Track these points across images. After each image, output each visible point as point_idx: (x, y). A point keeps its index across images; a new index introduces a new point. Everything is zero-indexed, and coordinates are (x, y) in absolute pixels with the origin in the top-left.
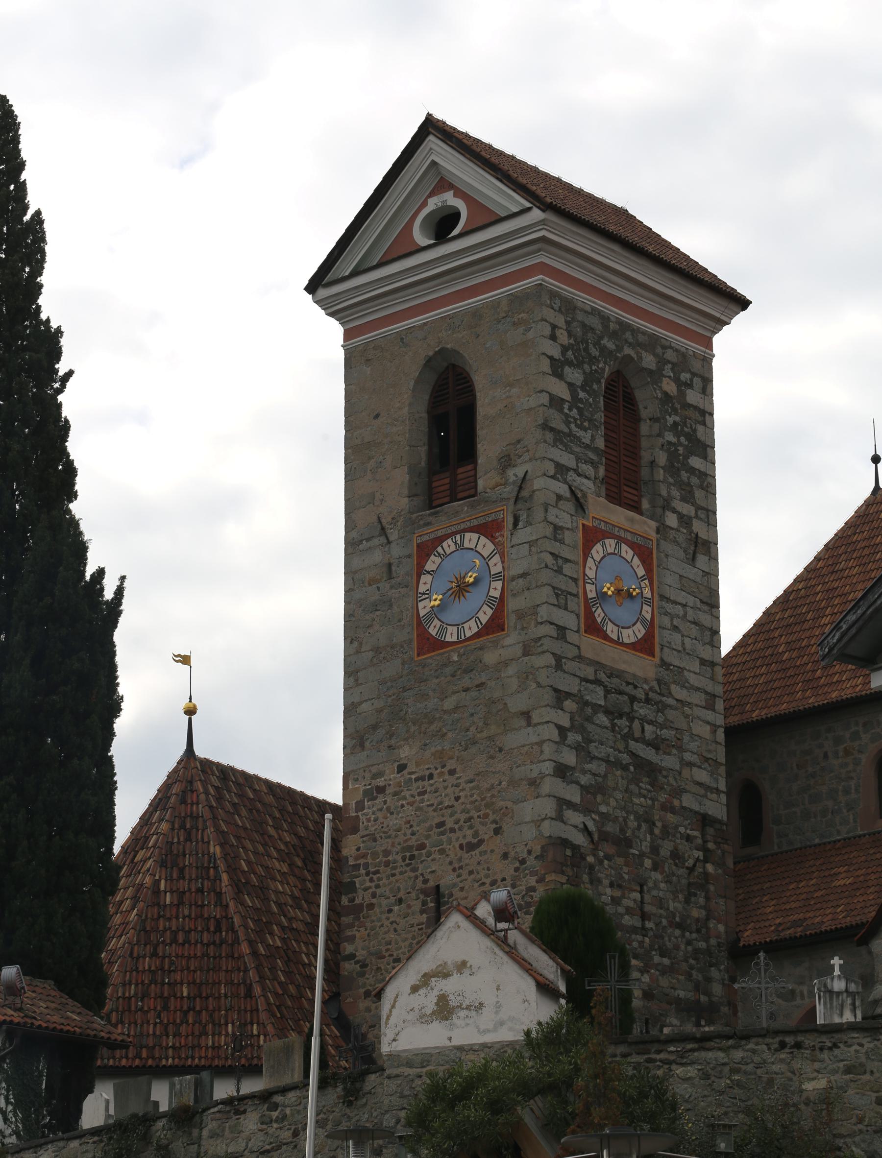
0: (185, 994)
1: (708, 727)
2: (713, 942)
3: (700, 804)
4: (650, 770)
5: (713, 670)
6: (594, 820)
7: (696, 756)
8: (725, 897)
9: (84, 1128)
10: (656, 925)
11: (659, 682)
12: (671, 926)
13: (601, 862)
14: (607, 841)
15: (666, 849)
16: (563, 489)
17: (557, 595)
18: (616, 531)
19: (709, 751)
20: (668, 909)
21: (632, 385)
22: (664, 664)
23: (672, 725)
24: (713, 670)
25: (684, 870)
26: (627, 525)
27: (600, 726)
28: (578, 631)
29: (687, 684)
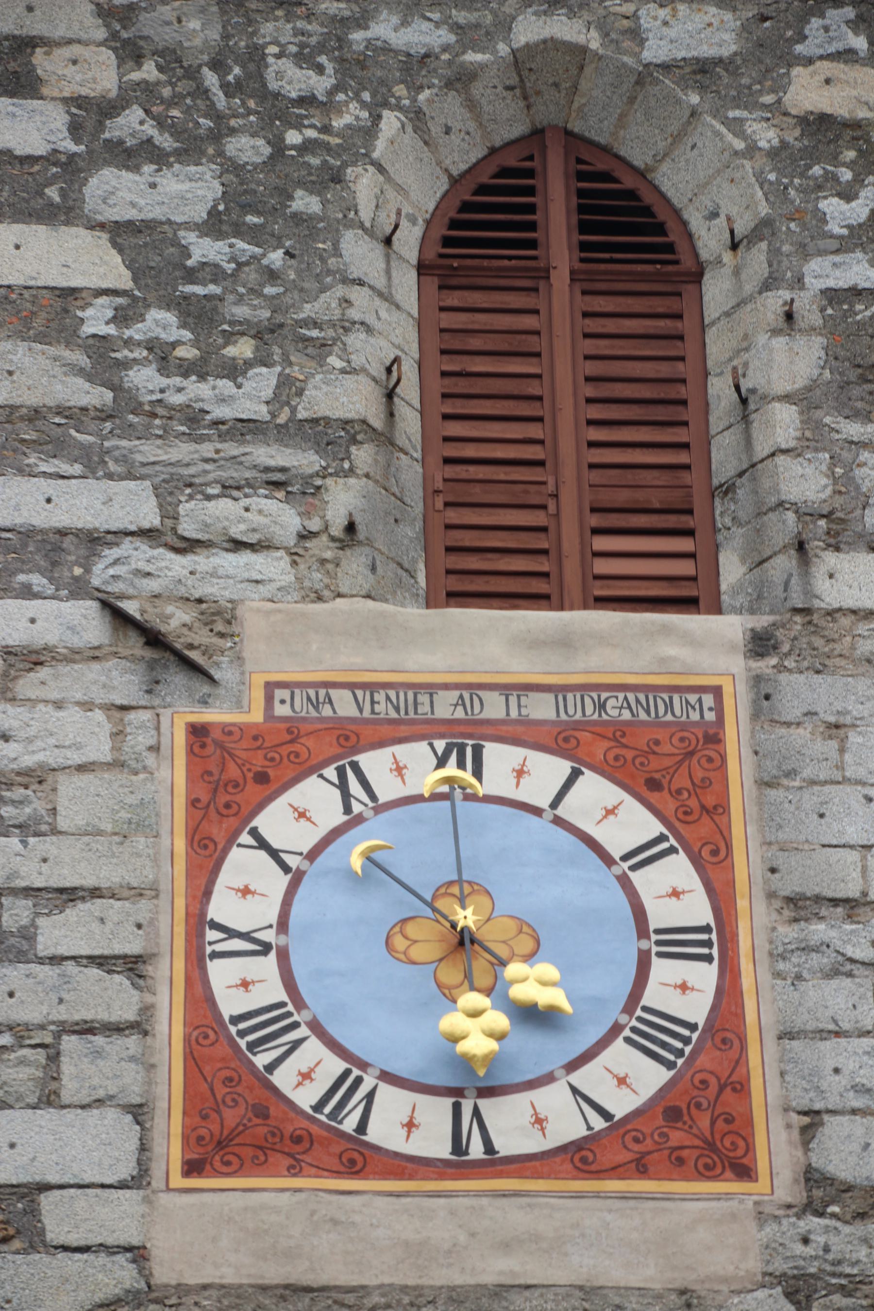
18: (494, 707)
26: (521, 668)
28: (139, 1180)
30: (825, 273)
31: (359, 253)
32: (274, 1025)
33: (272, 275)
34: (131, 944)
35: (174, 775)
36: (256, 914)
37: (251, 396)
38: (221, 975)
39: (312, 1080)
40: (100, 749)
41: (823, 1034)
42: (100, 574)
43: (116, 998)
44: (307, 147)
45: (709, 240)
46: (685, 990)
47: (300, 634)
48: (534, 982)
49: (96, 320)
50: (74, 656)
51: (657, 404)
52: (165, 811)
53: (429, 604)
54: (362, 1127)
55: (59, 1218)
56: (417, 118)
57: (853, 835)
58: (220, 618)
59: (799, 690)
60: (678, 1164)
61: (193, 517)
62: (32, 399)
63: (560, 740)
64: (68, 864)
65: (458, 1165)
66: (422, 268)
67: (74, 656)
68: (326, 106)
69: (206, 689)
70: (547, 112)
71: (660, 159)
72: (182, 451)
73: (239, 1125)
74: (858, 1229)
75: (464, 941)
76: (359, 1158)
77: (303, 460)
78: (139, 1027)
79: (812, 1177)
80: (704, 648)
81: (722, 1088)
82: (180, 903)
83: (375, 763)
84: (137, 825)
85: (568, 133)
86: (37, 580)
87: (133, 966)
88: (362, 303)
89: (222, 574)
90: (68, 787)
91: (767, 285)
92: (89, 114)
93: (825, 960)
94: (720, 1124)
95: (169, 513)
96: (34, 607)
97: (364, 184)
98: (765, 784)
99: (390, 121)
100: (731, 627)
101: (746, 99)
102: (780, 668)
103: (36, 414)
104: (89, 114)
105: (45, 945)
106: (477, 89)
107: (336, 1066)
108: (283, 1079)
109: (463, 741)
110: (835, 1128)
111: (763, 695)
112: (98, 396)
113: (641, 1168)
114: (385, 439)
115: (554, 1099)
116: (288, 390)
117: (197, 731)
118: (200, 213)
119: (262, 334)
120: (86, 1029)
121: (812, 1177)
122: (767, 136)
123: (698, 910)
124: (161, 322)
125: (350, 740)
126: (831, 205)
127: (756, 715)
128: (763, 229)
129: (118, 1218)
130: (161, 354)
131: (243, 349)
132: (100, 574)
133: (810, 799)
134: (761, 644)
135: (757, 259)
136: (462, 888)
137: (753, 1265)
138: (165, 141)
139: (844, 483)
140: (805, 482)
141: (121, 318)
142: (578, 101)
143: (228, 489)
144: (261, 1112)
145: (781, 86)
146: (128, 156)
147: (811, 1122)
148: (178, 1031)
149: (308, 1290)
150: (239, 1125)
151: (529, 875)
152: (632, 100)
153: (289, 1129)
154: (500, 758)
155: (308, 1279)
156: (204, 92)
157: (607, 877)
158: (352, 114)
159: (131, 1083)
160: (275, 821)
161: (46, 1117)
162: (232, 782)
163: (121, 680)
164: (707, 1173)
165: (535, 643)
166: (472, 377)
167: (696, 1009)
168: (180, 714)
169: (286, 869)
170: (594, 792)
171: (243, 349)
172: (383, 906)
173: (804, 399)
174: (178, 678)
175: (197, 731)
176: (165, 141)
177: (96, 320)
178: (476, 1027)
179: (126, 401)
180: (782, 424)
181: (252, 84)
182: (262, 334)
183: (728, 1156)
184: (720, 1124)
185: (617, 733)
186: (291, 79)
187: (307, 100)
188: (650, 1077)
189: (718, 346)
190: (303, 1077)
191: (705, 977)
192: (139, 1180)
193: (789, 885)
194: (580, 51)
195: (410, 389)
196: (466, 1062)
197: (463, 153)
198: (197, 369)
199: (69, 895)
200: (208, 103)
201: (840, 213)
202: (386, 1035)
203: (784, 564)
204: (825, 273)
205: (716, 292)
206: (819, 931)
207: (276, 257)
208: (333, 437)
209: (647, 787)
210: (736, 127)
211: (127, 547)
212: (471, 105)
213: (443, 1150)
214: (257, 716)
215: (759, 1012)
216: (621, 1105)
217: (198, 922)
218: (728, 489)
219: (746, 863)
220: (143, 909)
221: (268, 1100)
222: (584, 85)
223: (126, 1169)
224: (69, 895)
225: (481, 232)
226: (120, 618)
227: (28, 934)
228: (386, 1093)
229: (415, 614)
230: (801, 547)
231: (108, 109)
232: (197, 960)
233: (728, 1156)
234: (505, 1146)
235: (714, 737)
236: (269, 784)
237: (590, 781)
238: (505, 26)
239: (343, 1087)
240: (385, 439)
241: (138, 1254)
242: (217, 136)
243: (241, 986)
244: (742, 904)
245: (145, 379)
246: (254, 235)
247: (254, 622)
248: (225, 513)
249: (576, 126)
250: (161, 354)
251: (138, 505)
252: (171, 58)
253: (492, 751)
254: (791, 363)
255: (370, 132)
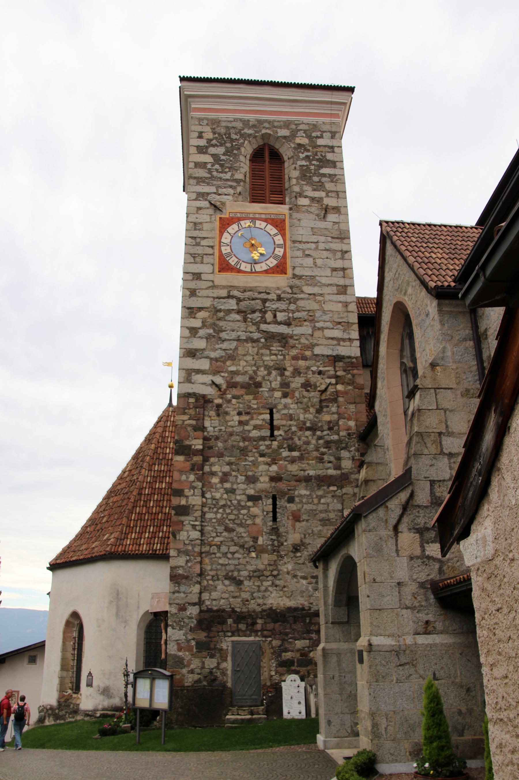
0: (133, 518)
1: (340, 305)
2: (343, 433)
3: (333, 350)
4: (283, 340)
5: (344, 273)
6: (223, 377)
7: (329, 323)
8: (355, 403)
9: (48, 609)
10: (286, 432)
11: (291, 287)
12: (300, 430)
13: (229, 401)
14: (236, 387)
15: (297, 382)
16: (206, 204)
17: (194, 257)
18: (257, 216)
19: (342, 318)
20: (298, 419)
21: (277, 147)
22: (295, 276)
23: (304, 309)
24: (344, 273)
25: (317, 393)
26: (261, 211)
27: (233, 321)
28: (213, 273)
29: (319, 284)
30: (300, 163)
31: (242, 158)
32: (229, 255)
33: (231, 161)
34: (212, 244)
35: (217, 223)
36: (227, 241)
37: (228, 176)
38: (223, 248)
40: (208, 220)
42: (209, 198)
43: (210, 251)
44: (236, 145)
45: (286, 158)
46: (280, 252)
47: (234, 206)
48: (262, 250)
49: (209, 166)
50: (205, 208)
51: (279, 178)
53: (250, 202)
55: (203, 277)
56: (250, 142)
57: (301, 233)
58: (223, 204)
59: (295, 215)
60: (278, 273)
61: (221, 191)
62: (201, 176)
63: (265, 220)
65: (251, 272)
66: (250, 160)
67: (205, 208)
68: (239, 140)
70: (266, 142)
72: (219, 183)
73: (225, 266)
75: (253, 245)
76: (239, 271)
77: (234, 184)
78: (213, 254)
79: (294, 274)
80: (283, 209)
83: (242, 223)
84: (213, 229)
86: (201, 199)
87: (212, 247)
88: (242, 165)
89: (224, 198)
90: (204, 225)
91: (293, 164)
92: (209, 141)
95: (217, 191)
97: (243, 149)
98: (291, 226)
99: (246, 142)
100: (287, 207)
101: (290, 141)
103: (201, 178)
104: (209, 141)
105: (202, 244)
107: (237, 260)
108: (230, 261)
109: (253, 220)
110: (297, 269)
111: (291, 215)
112: (209, 176)
113: (273, 273)
114: (245, 182)
115: (263, 265)
116: (233, 175)
117: (220, 218)
118: (222, 153)
119: (230, 168)
120: (207, 255)
121: (294, 274)
122: (293, 146)
123: (282, 242)
124: (217, 166)
125: (239, 219)
126: (301, 155)
128: (292, 157)
129: (211, 277)
130: (217, 170)
131: (227, 170)
132: (209, 198)
133: (296, 229)
134: (291, 209)
135: (291, 161)
136: (252, 239)
137: (286, 285)
138: (218, 144)
139: (301, 189)
140: (297, 189)
141: (212, 166)
143: (225, 187)
144: (228, 265)
145: (295, 140)
146: (214, 146)
147: (294, 268)
150: (225, 266)
151: (260, 237)
154: (258, 223)
156: (223, 138)
157: (271, 238)
158: (241, 141)
159: (212, 261)
160: (230, 229)
162: (225, 224)
163: (211, 211)
164: (281, 274)
165: (262, 208)
166: (256, 174)
167: (281, 254)
168: (218, 216)
170: (269, 227)
171: (227, 170)
172: (243, 241)
173: (297, 178)
174: (218, 211)
175: (220, 218)
176: (218, 144)
177: (209, 166)
178: (256, 256)
179: (212, 176)
180: (294, 181)
181: (229, 137)
182: (230, 168)
183: (284, 272)
185: (272, 220)
186: (234, 136)
187: (236, 139)
188: (275, 262)
189: (286, 171)
190: (233, 261)
191: (282, 250)
192: (213, 273)
193: (293, 239)
194: (270, 134)
195: (248, 175)
196: (255, 260)
197: (255, 146)
198: (221, 172)
199: (204, 238)
200: (205, 122)
201: (302, 156)
202: (244, 256)
203: (294, 199)
204: (300, 163)
205: (286, 165)
206: (296, 245)
207: (231, 158)
208: (238, 181)
209: (276, 226)
210: (289, 144)
211: (212, 195)
212: (256, 140)
213: (250, 270)
214: (228, 216)
215: (288, 255)
216: (271, 266)
217: (220, 242)
218: (287, 189)
220: (213, 240)
221: (228, 264)
223: (211, 271)
224: (204, 238)
225: (257, 156)
226: (211, 204)
227: (200, 243)
228: (243, 263)
229: (248, 204)
230: (296, 197)
231: (211, 140)
232: (220, 246)
233: (284, 272)
234: (257, 270)
235: (284, 220)
236: (229, 225)
237: (269, 225)
238: (261, 131)
239: (237, 263)
240: (245, 182)
241: (213, 281)
242: (225, 143)
243: (225, 250)
245: (215, 174)
246: (229, 156)
247: (228, 204)
248: (224, 191)
250: (217, 170)
251: (213, 189)
252: (219, 134)
253: (257, 221)
254: (295, 174)
255: (244, 143)
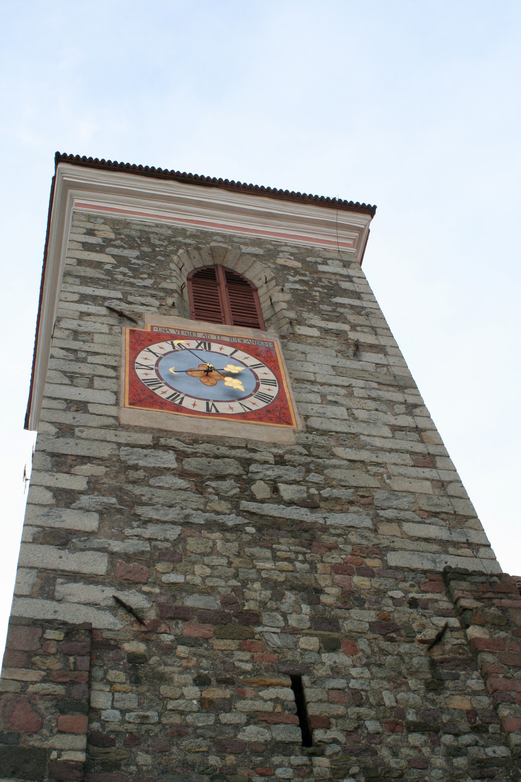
39: (406, 401)
41: (307, 402)
45: (257, 283)
52: (123, 343)
54: (181, 403)
58: (140, 315)
64: (95, 348)
69: (135, 325)
71: (245, 272)
74: (322, 437)
76: (179, 409)
81: (282, 408)
82: (128, 359)
85: (223, 267)
93: (307, 390)
94: (282, 415)
96: (89, 306)
102: (288, 341)
106: (202, 252)
113: (261, 419)
121: (307, 426)
127: (283, 348)
142: (225, 260)
147: (306, 417)
148: (127, 379)
149: (166, 431)
152: (239, 259)
153: (159, 401)
155: (166, 428)
161: (90, 390)
169: (157, 356)
184: (282, 415)
198: (134, 277)
199: (97, 354)
208: (169, 292)
210: (266, 264)
213: (204, 410)
214: (149, 330)
219: (283, 370)
220: (117, 358)
222: (227, 256)
224: (97, 354)
241: (116, 418)
244: (283, 378)
249: (225, 265)
